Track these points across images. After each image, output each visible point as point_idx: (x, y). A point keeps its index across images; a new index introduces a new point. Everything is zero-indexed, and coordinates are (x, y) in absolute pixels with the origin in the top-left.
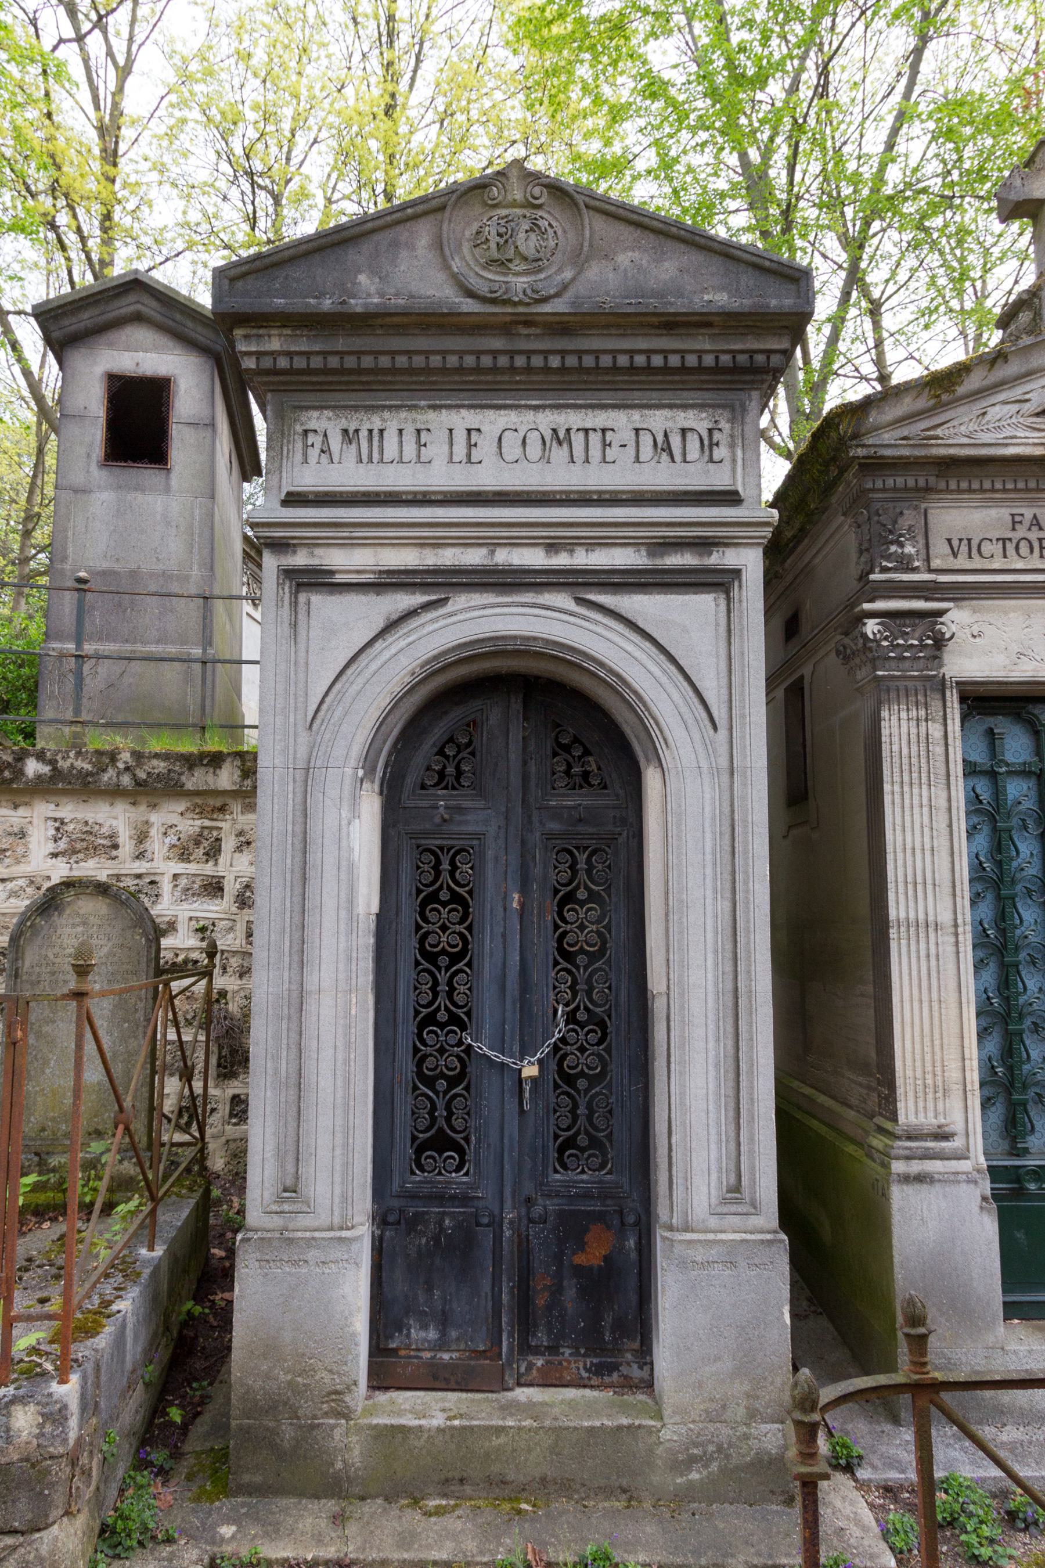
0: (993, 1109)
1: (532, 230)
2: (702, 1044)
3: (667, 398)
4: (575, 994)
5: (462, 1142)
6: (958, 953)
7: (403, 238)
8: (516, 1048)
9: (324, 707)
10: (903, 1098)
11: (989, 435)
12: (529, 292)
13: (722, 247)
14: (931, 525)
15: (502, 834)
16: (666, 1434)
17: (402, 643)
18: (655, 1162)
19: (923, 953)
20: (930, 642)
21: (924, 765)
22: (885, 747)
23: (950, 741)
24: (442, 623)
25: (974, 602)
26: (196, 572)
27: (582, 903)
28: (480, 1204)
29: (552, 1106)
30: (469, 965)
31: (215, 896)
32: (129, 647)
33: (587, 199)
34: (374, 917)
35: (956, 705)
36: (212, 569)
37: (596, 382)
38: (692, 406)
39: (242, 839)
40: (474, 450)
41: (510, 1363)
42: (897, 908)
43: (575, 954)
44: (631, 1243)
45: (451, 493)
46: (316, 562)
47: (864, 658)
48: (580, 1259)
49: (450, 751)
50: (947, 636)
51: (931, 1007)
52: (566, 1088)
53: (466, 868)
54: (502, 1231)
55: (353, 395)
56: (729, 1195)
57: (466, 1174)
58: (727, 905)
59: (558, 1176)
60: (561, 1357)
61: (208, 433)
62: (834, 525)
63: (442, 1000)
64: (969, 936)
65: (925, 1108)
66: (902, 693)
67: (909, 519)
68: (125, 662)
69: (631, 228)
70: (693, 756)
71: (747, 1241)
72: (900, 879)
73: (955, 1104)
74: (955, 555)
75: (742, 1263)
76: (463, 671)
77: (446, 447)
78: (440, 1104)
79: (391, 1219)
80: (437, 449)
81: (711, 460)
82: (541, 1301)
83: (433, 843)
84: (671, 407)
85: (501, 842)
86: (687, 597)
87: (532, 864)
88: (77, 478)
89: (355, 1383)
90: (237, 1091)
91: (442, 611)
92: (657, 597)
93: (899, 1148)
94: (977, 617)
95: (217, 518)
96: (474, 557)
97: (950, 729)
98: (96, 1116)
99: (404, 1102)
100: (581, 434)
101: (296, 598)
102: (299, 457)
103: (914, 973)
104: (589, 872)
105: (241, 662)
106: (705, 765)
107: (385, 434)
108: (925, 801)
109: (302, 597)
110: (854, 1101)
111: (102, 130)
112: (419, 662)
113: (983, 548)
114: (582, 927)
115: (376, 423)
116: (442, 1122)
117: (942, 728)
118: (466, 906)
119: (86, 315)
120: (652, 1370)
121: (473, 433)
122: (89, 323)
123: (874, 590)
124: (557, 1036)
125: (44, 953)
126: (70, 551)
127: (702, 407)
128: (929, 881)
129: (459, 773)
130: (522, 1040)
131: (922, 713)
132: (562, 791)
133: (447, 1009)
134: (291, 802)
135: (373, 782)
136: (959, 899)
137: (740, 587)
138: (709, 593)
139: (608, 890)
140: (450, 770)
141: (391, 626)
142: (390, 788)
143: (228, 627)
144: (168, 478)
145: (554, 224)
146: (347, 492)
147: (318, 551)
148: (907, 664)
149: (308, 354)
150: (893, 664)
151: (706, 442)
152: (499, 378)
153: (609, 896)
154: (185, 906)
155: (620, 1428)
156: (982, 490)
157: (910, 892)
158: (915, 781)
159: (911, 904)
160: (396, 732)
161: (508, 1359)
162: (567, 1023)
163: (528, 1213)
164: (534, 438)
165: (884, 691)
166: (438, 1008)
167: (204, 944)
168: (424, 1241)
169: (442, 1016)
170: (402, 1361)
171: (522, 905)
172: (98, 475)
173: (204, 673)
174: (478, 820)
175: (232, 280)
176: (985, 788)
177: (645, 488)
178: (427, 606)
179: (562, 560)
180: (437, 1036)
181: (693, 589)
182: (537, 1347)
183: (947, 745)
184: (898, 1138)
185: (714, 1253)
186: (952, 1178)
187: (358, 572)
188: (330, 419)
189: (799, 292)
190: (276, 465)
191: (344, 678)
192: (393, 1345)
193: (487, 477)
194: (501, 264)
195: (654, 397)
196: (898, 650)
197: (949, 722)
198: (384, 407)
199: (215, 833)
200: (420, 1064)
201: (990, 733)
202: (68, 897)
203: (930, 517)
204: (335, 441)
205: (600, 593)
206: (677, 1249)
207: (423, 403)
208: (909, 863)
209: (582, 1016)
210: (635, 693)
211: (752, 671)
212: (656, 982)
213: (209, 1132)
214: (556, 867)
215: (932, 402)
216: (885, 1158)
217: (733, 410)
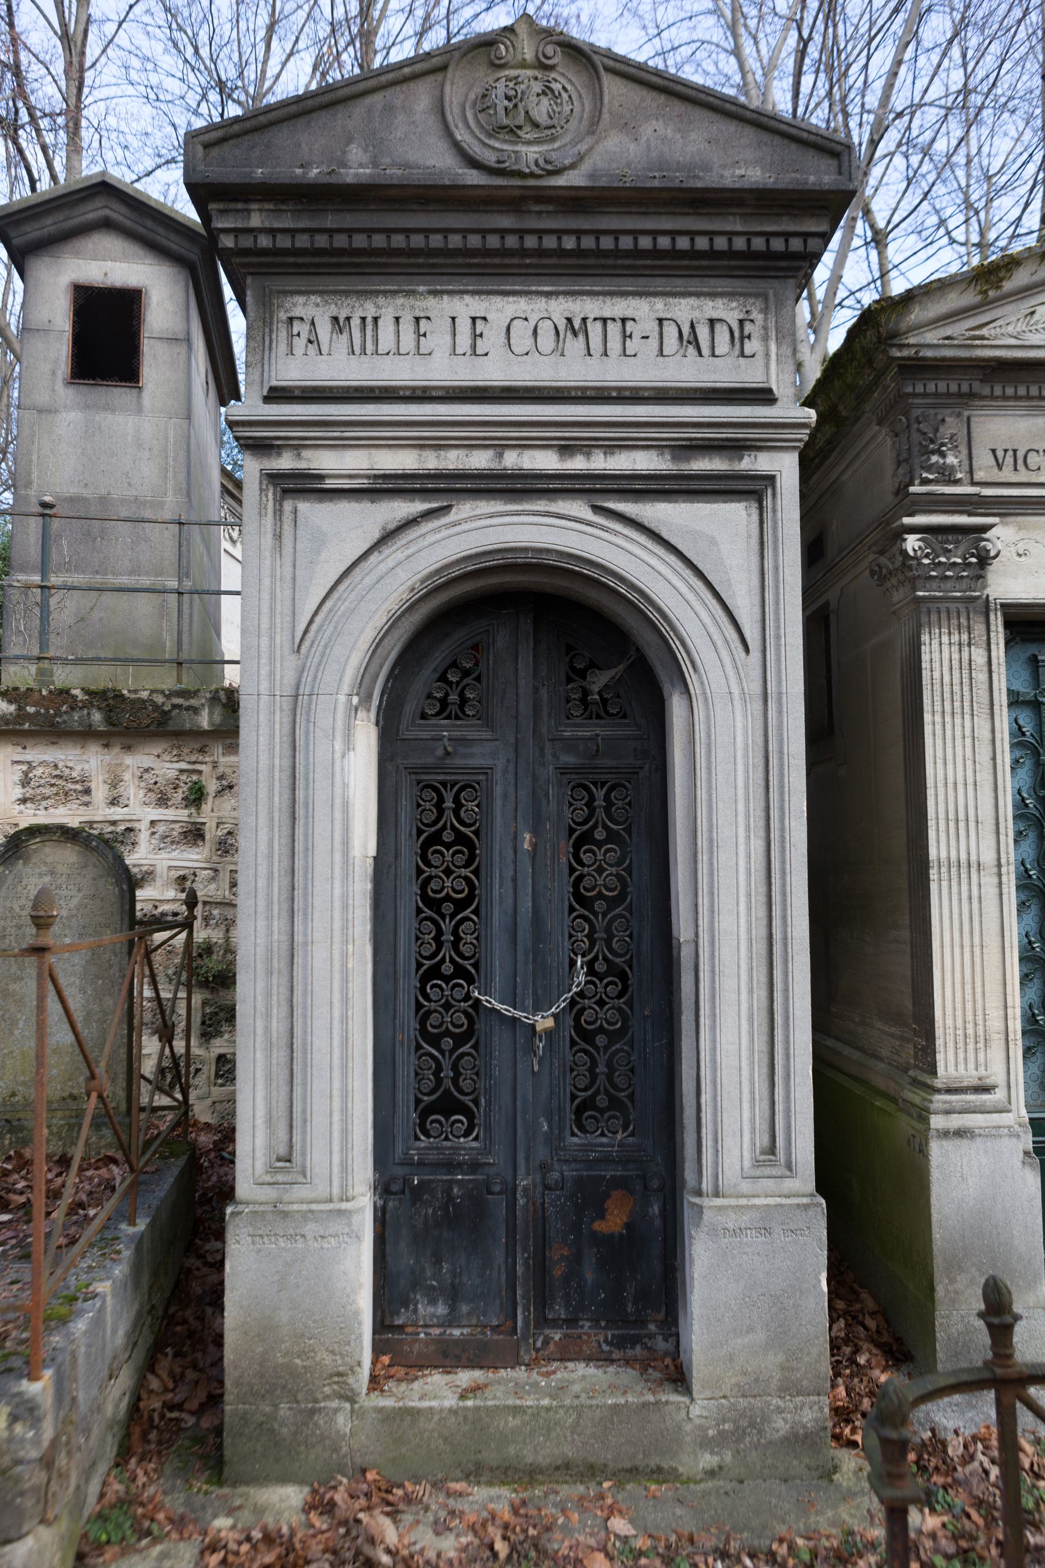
0: (1033, 1059)
1: (544, 93)
2: (734, 996)
3: (694, 284)
4: (593, 943)
5: (471, 1104)
6: (1001, 894)
7: (398, 103)
8: (529, 1002)
9: (314, 627)
10: (942, 1049)
11: (1038, 336)
12: (541, 162)
13: (755, 116)
14: (974, 434)
15: (511, 768)
16: (696, 1411)
17: (400, 556)
18: (682, 1123)
19: (965, 895)
20: (974, 560)
21: (967, 694)
22: (926, 674)
23: (994, 667)
24: (445, 533)
25: (1020, 519)
26: (170, 498)
27: (599, 844)
28: (492, 1171)
29: (568, 1064)
30: (476, 912)
31: (195, 844)
32: (98, 578)
33: (606, 60)
34: (370, 861)
35: (1001, 629)
36: (189, 495)
37: (615, 267)
38: (721, 295)
39: (225, 783)
40: (479, 340)
41: (525, 1337)
42: (937, 848)
43: (593, 900)
44: (655, 1209)
45: (454, 388)
46: (303, 465)
47: (902, 577)
48: (598, 1226)
49: (453, 678)
50: (992, 554)
51: (972, 952)
52: (584, 1045)
53: (471, 805)
54: (515, 1199)
55: (341, 279)
56: (763, 1157)
57: (476, 1139)
58: (757, 845)
59: (575, 1140)
60: (580, 1331)
61: (183, 349)
62: (867, 436)
63: (447, 951)
64: (1013, 876)
65: (966, 1059)
66: (944, 615)
67: (952, 426)
68: (95, 594)
69: (654, 94)
70: (724, 681)
71: (782, 1205)
72: (942, 816)
73: (996, 1054)
74: (1000, 467)
75: (777, 1230)
76: (468, 586)
77: (448, 338)
78: (446, 1064)
79: (395, 1188)
80: (438, 339)
81: (742, 354)
82: (558, 1271)
83: (435, 778)
84: (698, 295)
85: (511, 777)
86: (715, 506)
87: (544, 802)
88: (42, 398)
89: (359, 1364)
90: (222, 1051)
91: (444, 520)
92: (683, 505)
93: (938, 1101)
94: (1022, 534)
95: (193, 442)
96: (480, 460)
97: (994, 654)
98: (70, 1080)
99: (406, 1063)
100: (599, 325)
101: (281, 505)
102: (283, 347)
103: (956, 917)
104: (607, 810)
105: (220, 593)
106: (736, 691)
107: (380, 322)
108: (968, 732)
109: (288, 506)
110: (884, 1053)
111: (65, 37)
112: (419, 576)
113: (1029, 460)
114: (600, 870)
115: (369, 309)
116: (448, 1083)
117: (986, 654)
118: (472, 847)
119: (49, 221)
120: (678, 1342)
121: (479, 322)
122: (52, 229)
123: (914, 503)
124: (575, 990)
125: (8, 904)
126: (34, 476)
127: (731, 295)
128: (972, 818)
129: (463, 701)
130: (535, 993)
131: (965, 637)
132: (578, 721)
133: (452, 960)
134: (277, 733)
135: (369, 711)
136: (1002, 838)
137: (774, 495)
138: (739, 501)
139: (628, 830)
140: (453, 697)
141: (387, 537)
142: (386, 718)
143: (205, 558)
144: (139, 396)
145: (569, 87)
146: (338, 388)
147: (305, 453)
148: (949, 585)
149: (292, 232)
150: (934, 584)
151: (737, 334)
152: (507, 261)
153: (630, 837)
154: (164, 855)
155: (645, 1405)
156: (1028, 397)
157: (952, 830)
158: (958, 710)
159: (953, 842)
160: (393, 655)
161: (523, 1334)
162: (587, 974)
163: (544, 1179)
164: (546, 327)
165: (921, 614)
166: (443, 961)
167: (183, 896)
168: (430, 1211)
169: (447, 969)
170: (409, 1338)
171: (535, 846)
172: (66, 394)
173: (180, 604)
174: (481, 750)
175: (207, 146)
176: (1028, 720)
177: (669, 384)
178: (427, 515)
179: (578, 464)
180: (442, 990)
181: (722, 498)
182: (554, 1320)
183: (990, 672)
184: (938, 1091)
185: (745, 1219)
186: (994, 1132)
187: (350, 477)
188: (317, 305)
189: (840, 167)
190: (258, 357)
191: (336, 595)
192: (399, 1322)
193: (494, 371)
194: (512, 132)
195: (679, 284)
196: (940, 569)
197: (993, 647)
198: (378, 293)
199: (195, 778)
200: (423, 1021)
201: (1034, 661)
202: (34, 844)
203: (973, 426)
204: (324, 329)
205: (619, 501)
206: (707, 1215)
207: (421, 288)
208: (951, 799)
209: (600, 967)
210: (659, 610)
211: (787, 588)
212: (683, 931)
213: (193, 1095)
214: (571, 805)
215: (979, 298)
216: (923, 1115)
217: (766, 298)
